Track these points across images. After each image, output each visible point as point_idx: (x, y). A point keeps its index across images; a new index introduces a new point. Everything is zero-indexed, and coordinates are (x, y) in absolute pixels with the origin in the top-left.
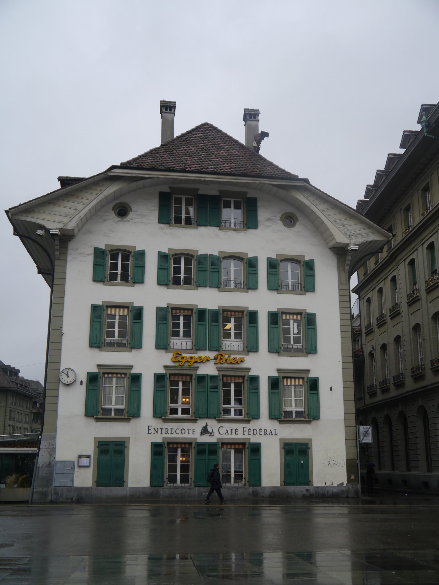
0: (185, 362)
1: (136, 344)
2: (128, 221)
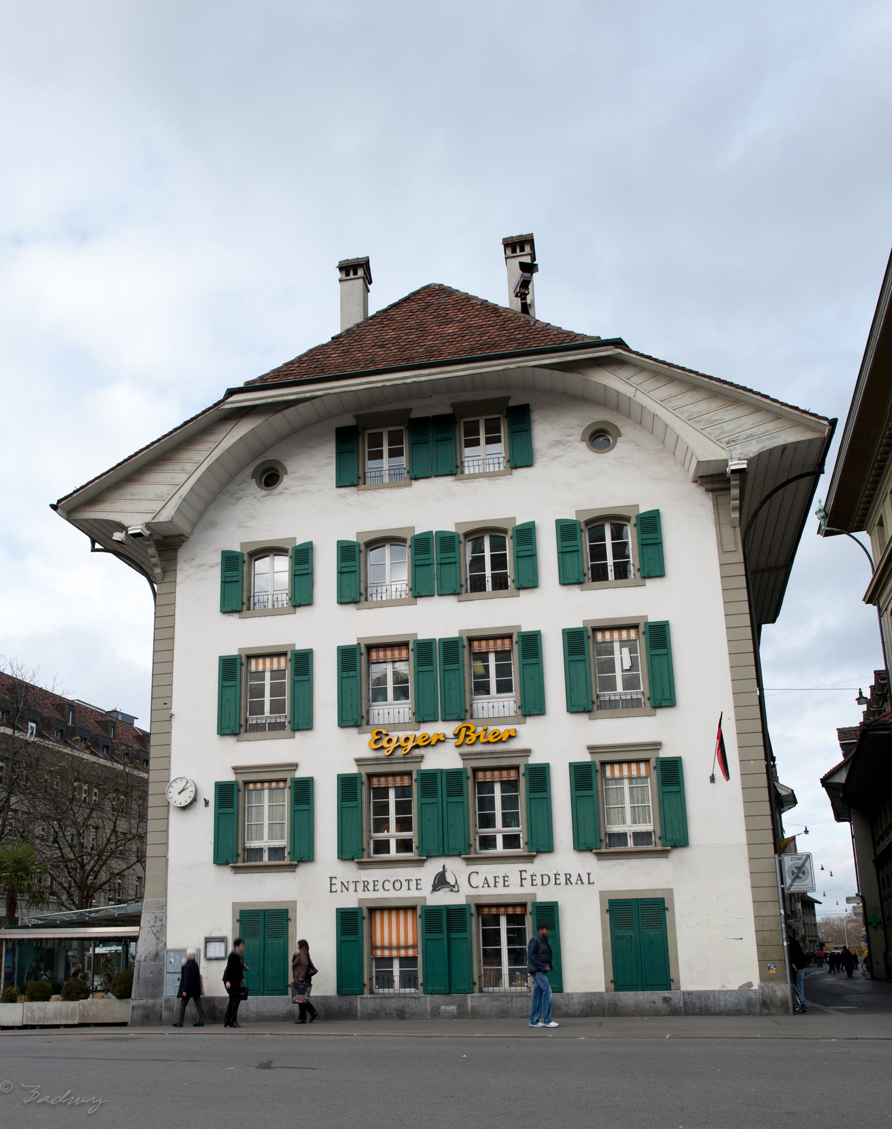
0: (396, 748)
1: (302, 721)
2: (280, 494)
